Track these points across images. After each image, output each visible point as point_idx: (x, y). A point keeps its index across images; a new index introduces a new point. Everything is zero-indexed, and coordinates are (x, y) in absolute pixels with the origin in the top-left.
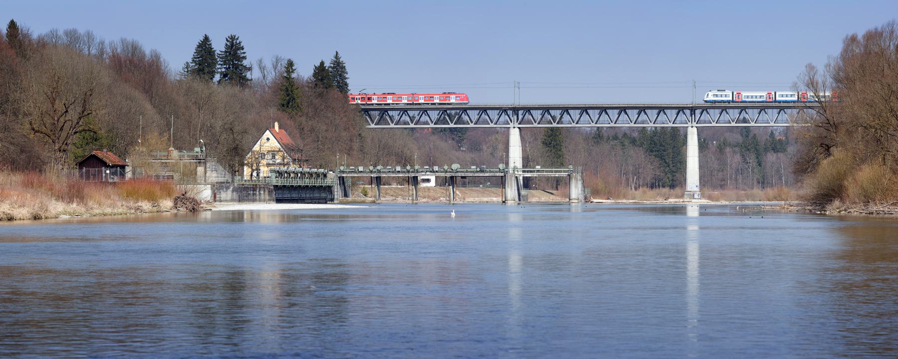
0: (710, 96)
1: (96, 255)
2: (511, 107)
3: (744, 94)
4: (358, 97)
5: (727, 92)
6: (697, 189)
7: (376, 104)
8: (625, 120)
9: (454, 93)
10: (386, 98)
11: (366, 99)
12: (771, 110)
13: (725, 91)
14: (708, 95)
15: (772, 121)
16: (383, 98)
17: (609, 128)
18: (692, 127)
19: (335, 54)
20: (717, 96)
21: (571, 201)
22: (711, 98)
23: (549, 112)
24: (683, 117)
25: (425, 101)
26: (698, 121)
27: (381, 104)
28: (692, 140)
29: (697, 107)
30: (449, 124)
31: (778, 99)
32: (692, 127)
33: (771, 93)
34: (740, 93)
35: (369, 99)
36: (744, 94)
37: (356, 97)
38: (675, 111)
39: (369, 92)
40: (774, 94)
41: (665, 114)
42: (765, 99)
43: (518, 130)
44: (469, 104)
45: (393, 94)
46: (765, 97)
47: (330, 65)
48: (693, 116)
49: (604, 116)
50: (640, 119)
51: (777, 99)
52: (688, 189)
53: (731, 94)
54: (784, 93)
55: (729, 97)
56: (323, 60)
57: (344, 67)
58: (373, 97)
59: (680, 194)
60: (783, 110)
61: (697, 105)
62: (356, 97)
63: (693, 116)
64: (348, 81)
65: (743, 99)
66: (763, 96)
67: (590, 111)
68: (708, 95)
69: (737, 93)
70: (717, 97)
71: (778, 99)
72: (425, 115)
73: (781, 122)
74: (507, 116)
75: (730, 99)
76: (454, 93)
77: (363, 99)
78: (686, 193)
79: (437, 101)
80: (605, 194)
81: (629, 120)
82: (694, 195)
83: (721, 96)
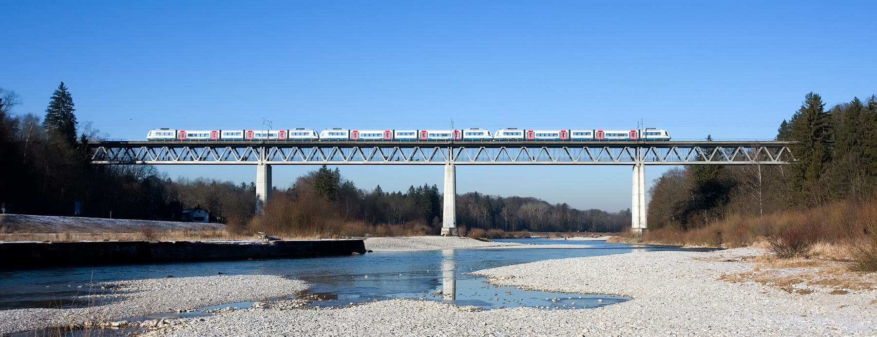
0: (500, 134)
1: (27, 221)
3: (361, 132)
5: (481, 130)
14: (151, 133)
17: (769, 166)
18: (450, 164)
20: (333, 134)
21: (222, 210)
34: (425, 132)
36: (255, 132)
40: (392, 132)
46: (210, 135)
50: (415, 157)
51: (395, 137)
54: (260, 132)
56: (70, 90)
57: (71, 99)
64: (74, 113)
66: (208, 134)
68: (151, 133)
70: (333, 135)
71: (223, 137)
75: (174, 137)
83: (337, 134)
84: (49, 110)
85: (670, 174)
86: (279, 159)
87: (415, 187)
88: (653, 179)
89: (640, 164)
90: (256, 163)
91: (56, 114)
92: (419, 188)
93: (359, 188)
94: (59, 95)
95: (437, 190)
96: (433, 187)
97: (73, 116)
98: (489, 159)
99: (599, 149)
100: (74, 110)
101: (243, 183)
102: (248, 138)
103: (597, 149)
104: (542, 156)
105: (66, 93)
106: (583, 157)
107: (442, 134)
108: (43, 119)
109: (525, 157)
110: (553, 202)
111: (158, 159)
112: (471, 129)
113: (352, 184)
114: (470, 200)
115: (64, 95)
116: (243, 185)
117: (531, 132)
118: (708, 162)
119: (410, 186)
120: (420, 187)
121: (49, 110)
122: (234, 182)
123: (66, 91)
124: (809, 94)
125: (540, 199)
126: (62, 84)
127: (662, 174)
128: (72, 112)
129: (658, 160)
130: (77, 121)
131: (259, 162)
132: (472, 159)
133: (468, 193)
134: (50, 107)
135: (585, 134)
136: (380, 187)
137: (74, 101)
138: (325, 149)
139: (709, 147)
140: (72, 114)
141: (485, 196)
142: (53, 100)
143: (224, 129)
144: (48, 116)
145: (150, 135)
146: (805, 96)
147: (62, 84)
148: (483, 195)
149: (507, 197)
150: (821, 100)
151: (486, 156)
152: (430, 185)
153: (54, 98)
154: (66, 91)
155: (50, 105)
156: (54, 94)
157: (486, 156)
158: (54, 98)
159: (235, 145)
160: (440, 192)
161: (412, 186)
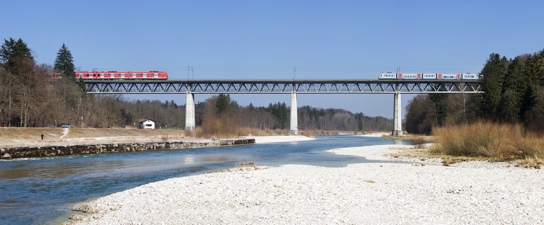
2: (186, 81)
3: (404, 75)
4: (91, 74)
6: (297, 129)
7: (104, 79)
8: (244, 89)
9: (157, 72)
10: (110, 74)
11: (97, 75)
12: (317, 84)
13: (392, 73)
15: (339, 90)
16: (108, 74)
18: (294, 93)
19: (5, 40)
22: (383, 77)
23: (244, 85)
24: (288, 87)
25: (115, 77)
26: (297, 90)
27: (107, 79)
28: (293, 100)
29: (296, 82)
30: (474, 91)
31: (424, 78)
32: (294, 93)
33: (420, 75)
35: (99, 75)
37: (90, 74)
38: (118, 85)
39: (99, 71)
40: (461, 75)
41: (267, 85)
42: (416, 78)
43: (191, 95)
44: (168, 80)
45: (115, 72)
46: (416, 77)
47: (59, 52)
48: (294, 87)
49: (243, 87)
51: (463, 78)
52: (291, 129)
53: (435, 75)
55: (425, 75)
56: (69, 48)
57: (70, 54)
58: (101, 74)
59: (286, 132)
60: (277, 83)
61: (296, 81)
62: (90, 74)
63: (294, 87)
64: (73, 63)
65: (403, 78)
67: (268, 85)
69: (439, 75)
71: (424, 78)
72: (210, 86)
73: (344, 91)
74: (233, 87)
76: (157, 72)
77: (94, 75)
78: (290, 131)
79: (145, 77)
80: (455, 124)
81: (245, 89)
82: (294, 132)
84: (57, 61)
85: (418, 98)
86: (172, 91)
87: (273, 104)
88: (408, 101)
89: (398, 93)
90: (185, 92)
91: (61, 64)
92: (275, 104)
93: (240, 105)
94: (62, 52)
95: (286, 105)
96: (283, 104)
97: (72, 65)
98: (326, 90)
99: (152, 84)
100: (73, 61)
101: (167, 101)
102: (399, 78)
103: (363, 84)
104: (344, 88)
105: (67, 51)
106: (366, 89)
107: (451, 76)
108: (53, 66)
109: (357, 89)
110: (354, 112)
111: (113, 91)
112: (387, 73)
113: (236, 102)
114: (304, 111)
115: (65, 51)
116: (166, 102)
117: (440, 75)
118: (437, 92)
119: (269, 104)
120: (276, 104)
121: (57, 61)
122: (161, 100)
123: (67, 49)
124: (492, 54)
125: (346, 110)
126: (64, 45)
127: (413, 98)
128: (71, 62)
129: (326, 90)
130: (75, 68)
131: (187, 92)
132: (317, 90)
133: (303, 106)
134: (57, 59)
135: (467, 76)
136: (252, 104)
137: (72, 56)
138: (201, 84)
139: (441, 84)
140: (72, 63)
141: (313, 108)
142: (59, 55)
143: (425, 73)
144: (57, 65)
145: (381, 77)
146: (490, 55)
147: (64, 45)
148: (312, 108)
149: (326, 109)
150: (500, 57)
151: (313, 89)
152: (282, 103)
153: (59, 54)
154: (67, 49)
155: (57, 58)
156: (59, 51)
157: (313, 89)
158: (59, 54)
159: (390, 82)
160: (287, 106)
161: (271, 103)
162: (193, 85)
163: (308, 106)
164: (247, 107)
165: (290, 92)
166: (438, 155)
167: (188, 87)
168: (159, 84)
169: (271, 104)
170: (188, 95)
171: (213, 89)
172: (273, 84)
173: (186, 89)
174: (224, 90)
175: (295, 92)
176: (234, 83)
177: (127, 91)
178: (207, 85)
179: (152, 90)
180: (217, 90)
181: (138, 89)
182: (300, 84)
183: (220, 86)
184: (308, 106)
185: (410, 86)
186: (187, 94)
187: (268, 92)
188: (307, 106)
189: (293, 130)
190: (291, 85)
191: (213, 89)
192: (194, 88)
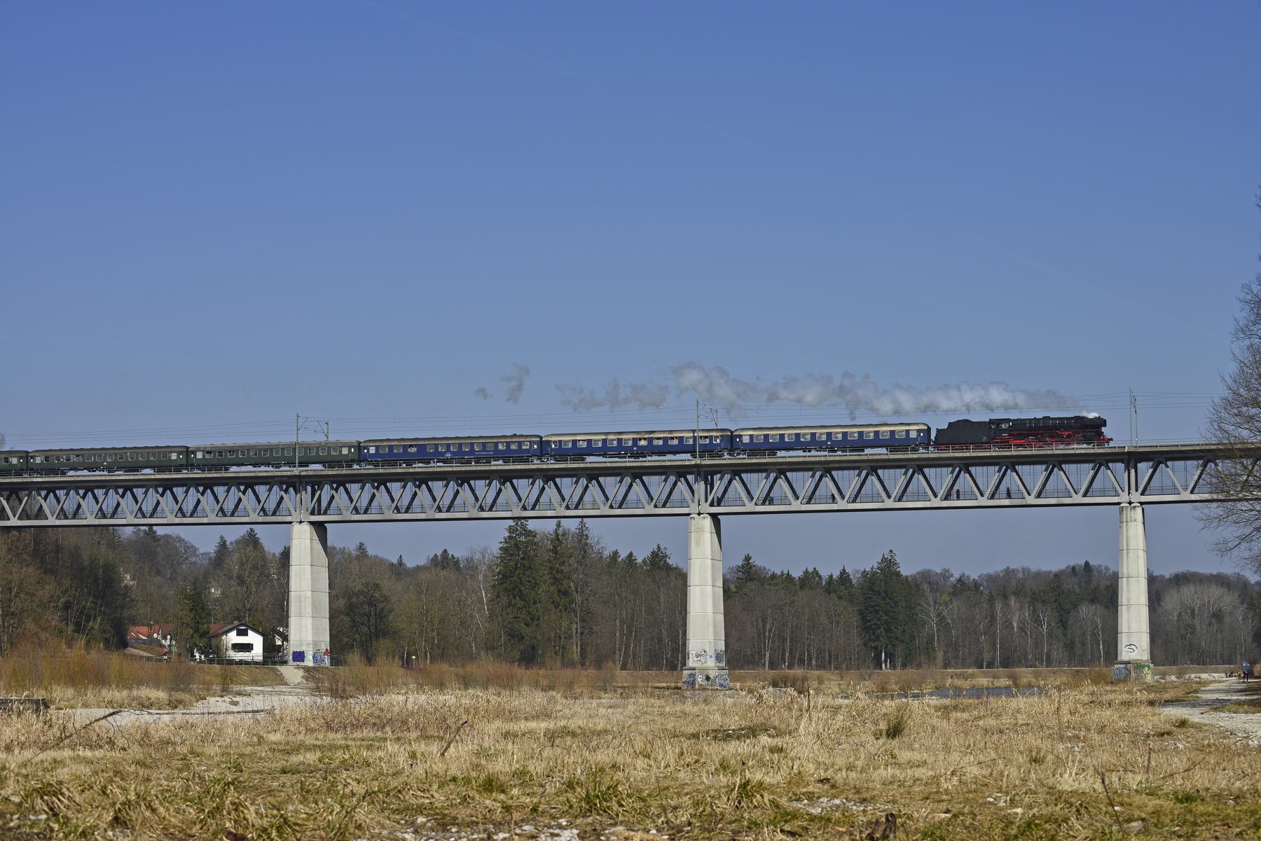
23: (1061, 467)
28: (698, 544)
30: (9, 519)
43: (708, 522)
48: (1133, 471)
63: (1133, 471)
74: (967, 475)
119: (443, 549)
132: (254, 512)
133: (1068, 567)
162: (717, 477)
163: (1087, 563)
164: (412, 568)
165: (1115, 500)
166: (1218, 797)
167: (695, 487)
168: (680, 477)
169: (888, 566)
170: (296, 527)
171: (748, 492)
172: (1091, 465)
173: (687, 494)
174: (883, 495)
175: (1136, 497)
176: (515, 478)
177: (398, 510)
178: (818, 474)
179: (567, 500)
180: (856, 496)
181: (563, 499)
182: (1101, 465)
183: (962, 472)
184: (1087, 563)
185: (1173, 472)
186: (296, 527)
187: (928, 504)
188: (1082, 563)
189: (694, 669)
190: (1120, 466)
191: (748, 492)
192: (719, 485)
